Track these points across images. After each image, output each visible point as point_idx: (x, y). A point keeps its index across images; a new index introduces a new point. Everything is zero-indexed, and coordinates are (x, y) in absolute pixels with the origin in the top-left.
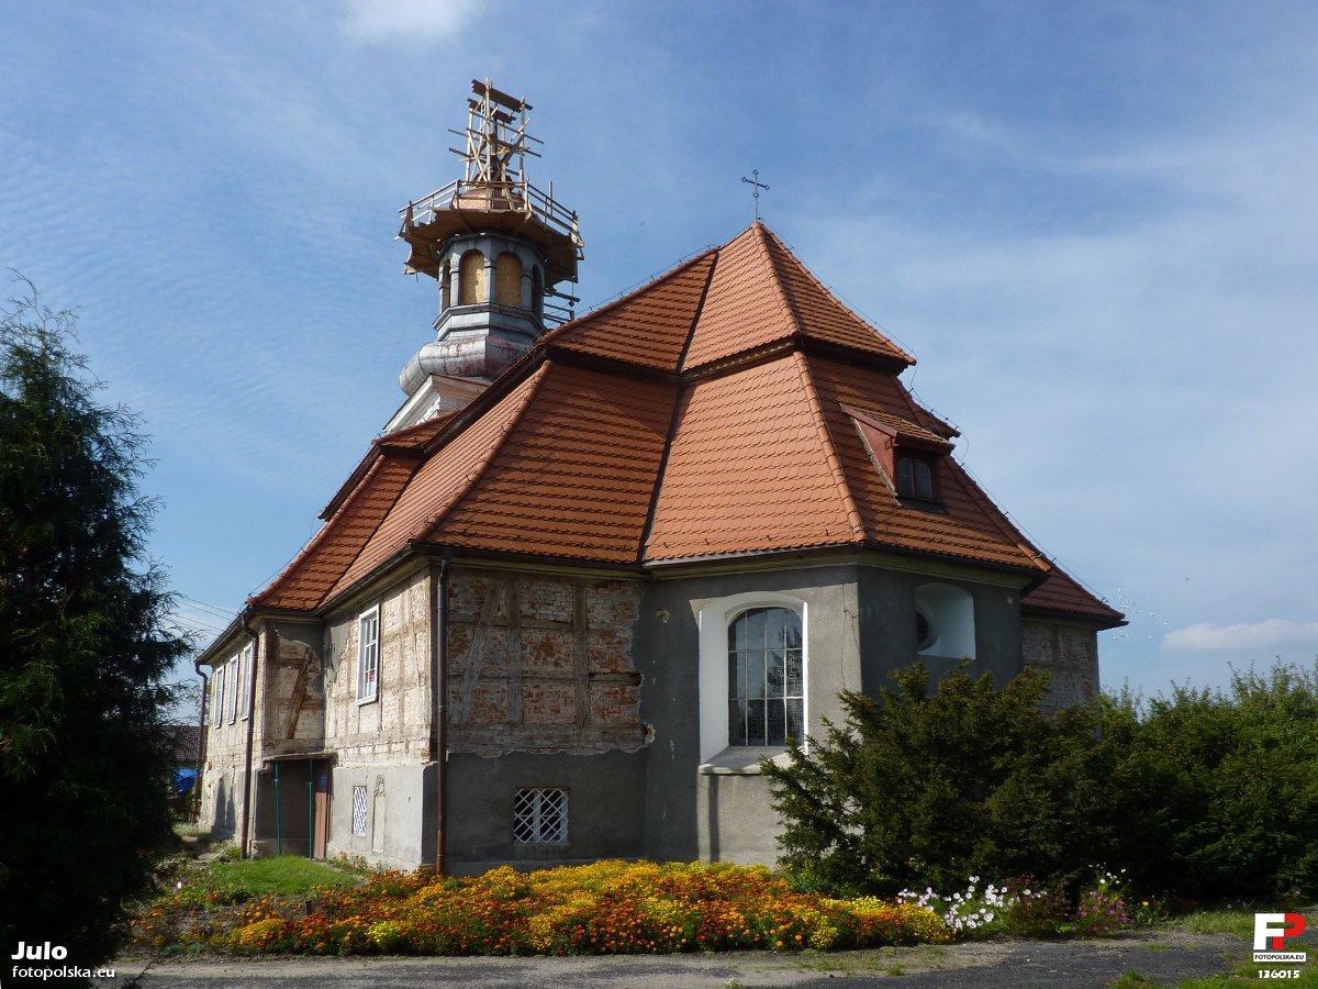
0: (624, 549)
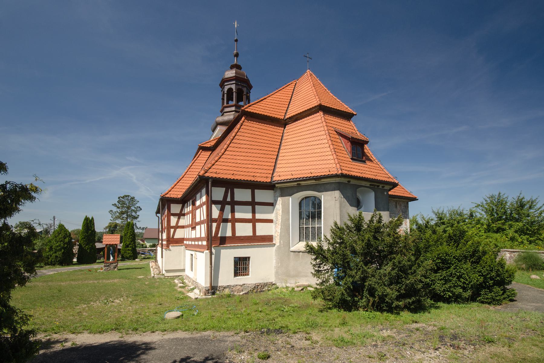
0: (267, 177)
